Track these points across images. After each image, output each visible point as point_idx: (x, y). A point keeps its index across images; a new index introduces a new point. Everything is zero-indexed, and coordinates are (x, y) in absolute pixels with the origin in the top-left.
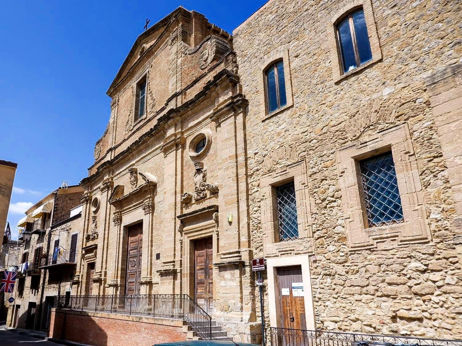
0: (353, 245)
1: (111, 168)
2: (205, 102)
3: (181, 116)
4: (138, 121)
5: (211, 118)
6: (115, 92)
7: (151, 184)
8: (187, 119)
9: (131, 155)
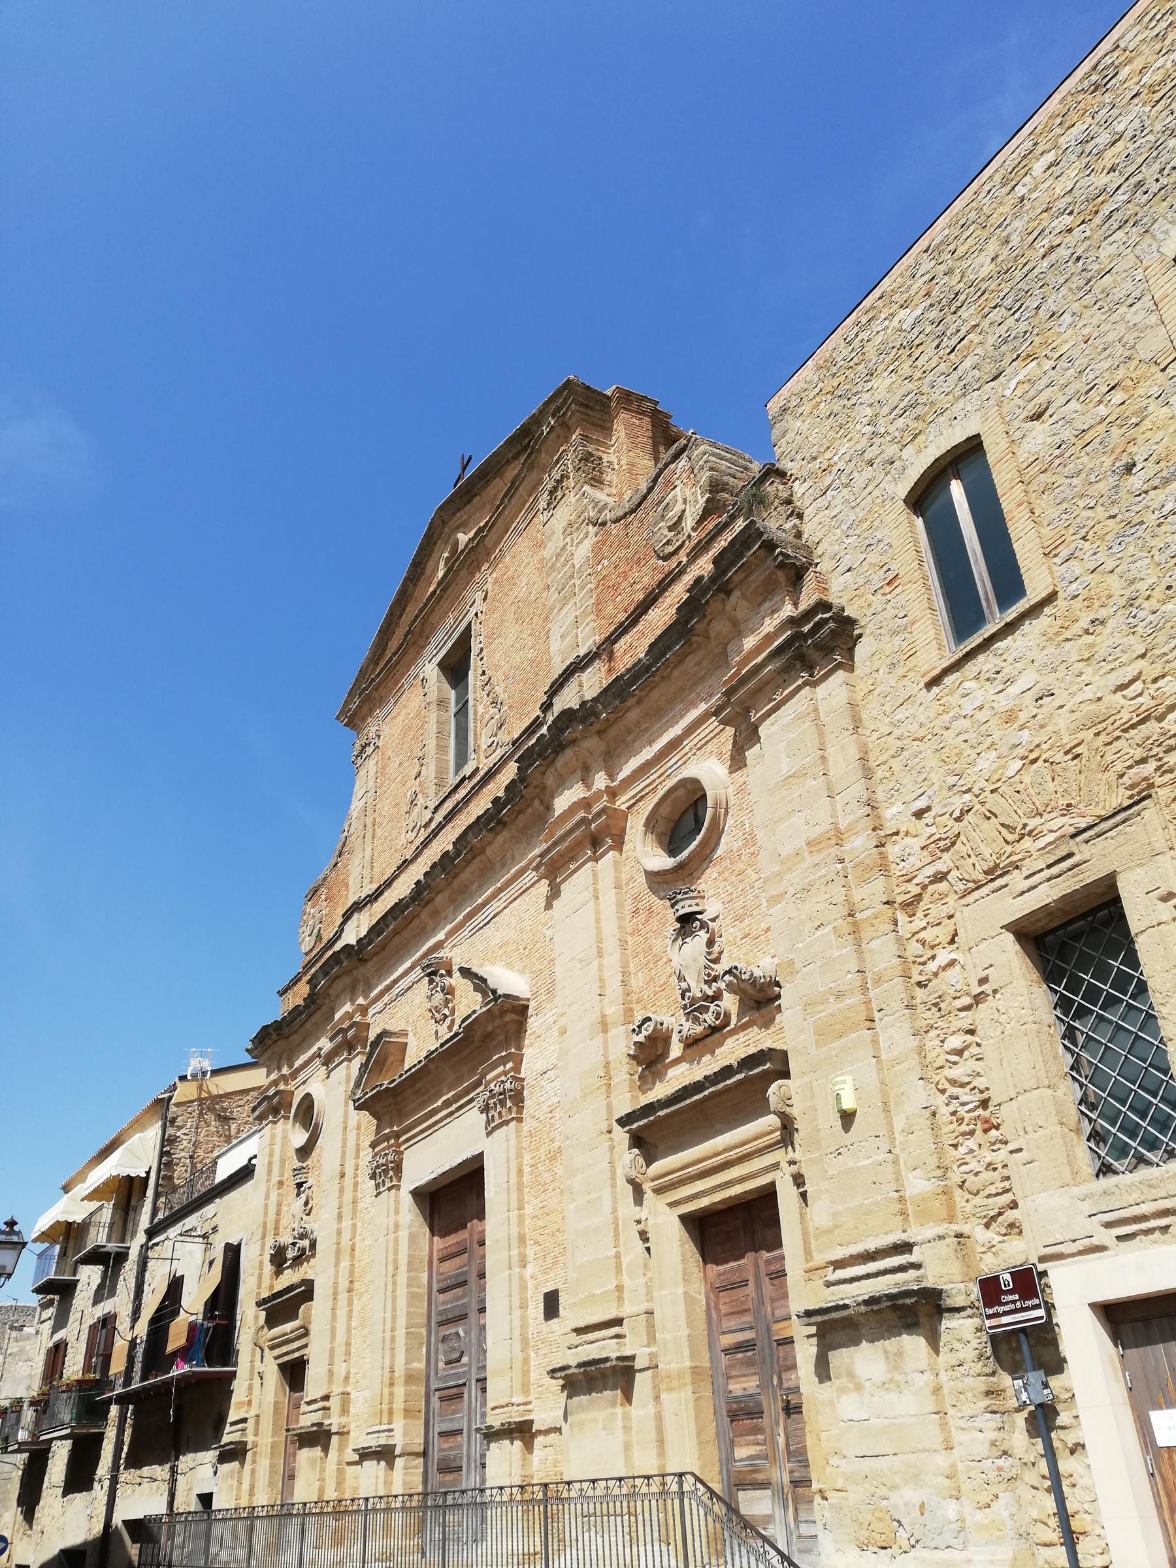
2: (690, 661)
3: (600, 733)
6: (365, 709)
7: (506, 1006)
8: (623, 741)
9: (427, 911)
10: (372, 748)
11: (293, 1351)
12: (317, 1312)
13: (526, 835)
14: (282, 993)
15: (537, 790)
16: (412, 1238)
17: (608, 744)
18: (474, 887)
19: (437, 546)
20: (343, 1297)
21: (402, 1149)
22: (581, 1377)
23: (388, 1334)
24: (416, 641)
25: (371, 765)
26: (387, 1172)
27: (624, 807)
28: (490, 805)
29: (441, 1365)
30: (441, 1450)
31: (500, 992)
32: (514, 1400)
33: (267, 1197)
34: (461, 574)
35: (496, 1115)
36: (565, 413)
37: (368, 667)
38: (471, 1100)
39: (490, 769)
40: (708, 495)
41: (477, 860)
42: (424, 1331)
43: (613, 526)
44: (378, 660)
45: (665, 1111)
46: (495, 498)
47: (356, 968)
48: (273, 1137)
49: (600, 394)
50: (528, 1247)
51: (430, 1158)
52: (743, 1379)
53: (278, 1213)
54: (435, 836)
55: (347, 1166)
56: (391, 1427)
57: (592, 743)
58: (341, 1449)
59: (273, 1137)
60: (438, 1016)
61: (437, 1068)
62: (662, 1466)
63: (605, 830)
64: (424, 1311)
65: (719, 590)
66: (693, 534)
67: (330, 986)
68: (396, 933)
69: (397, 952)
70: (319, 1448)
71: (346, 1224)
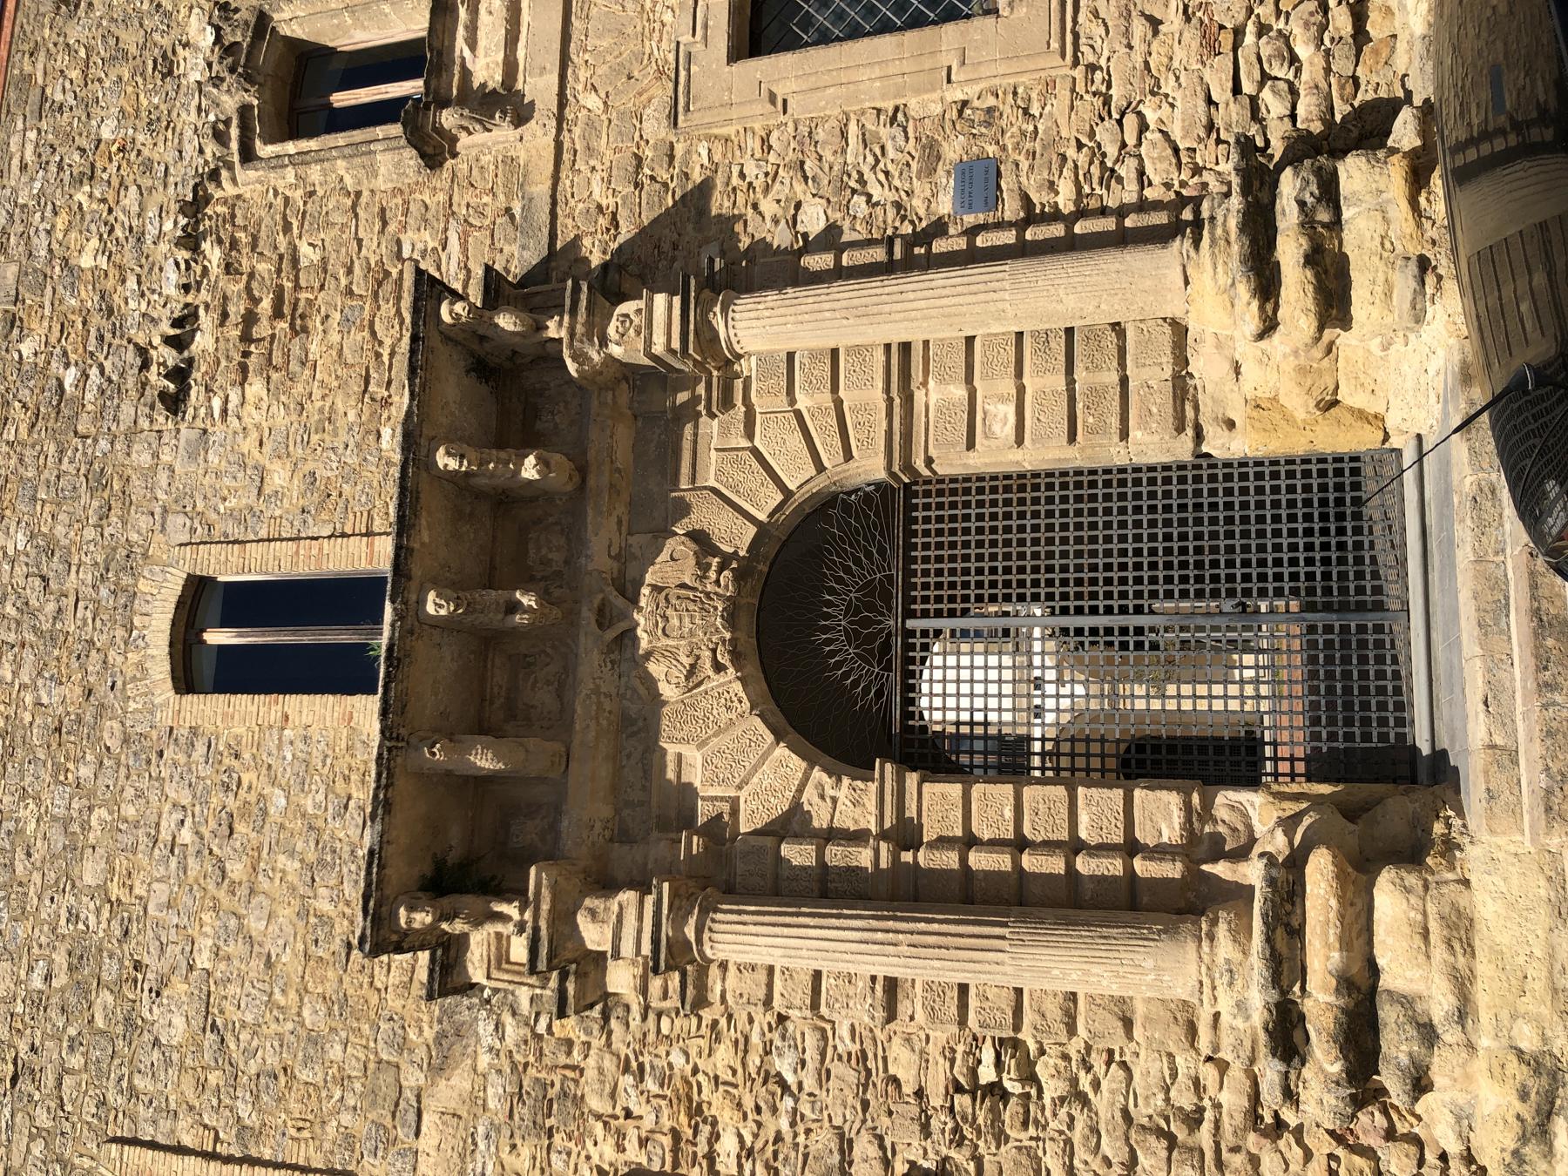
0: (1055, 45)
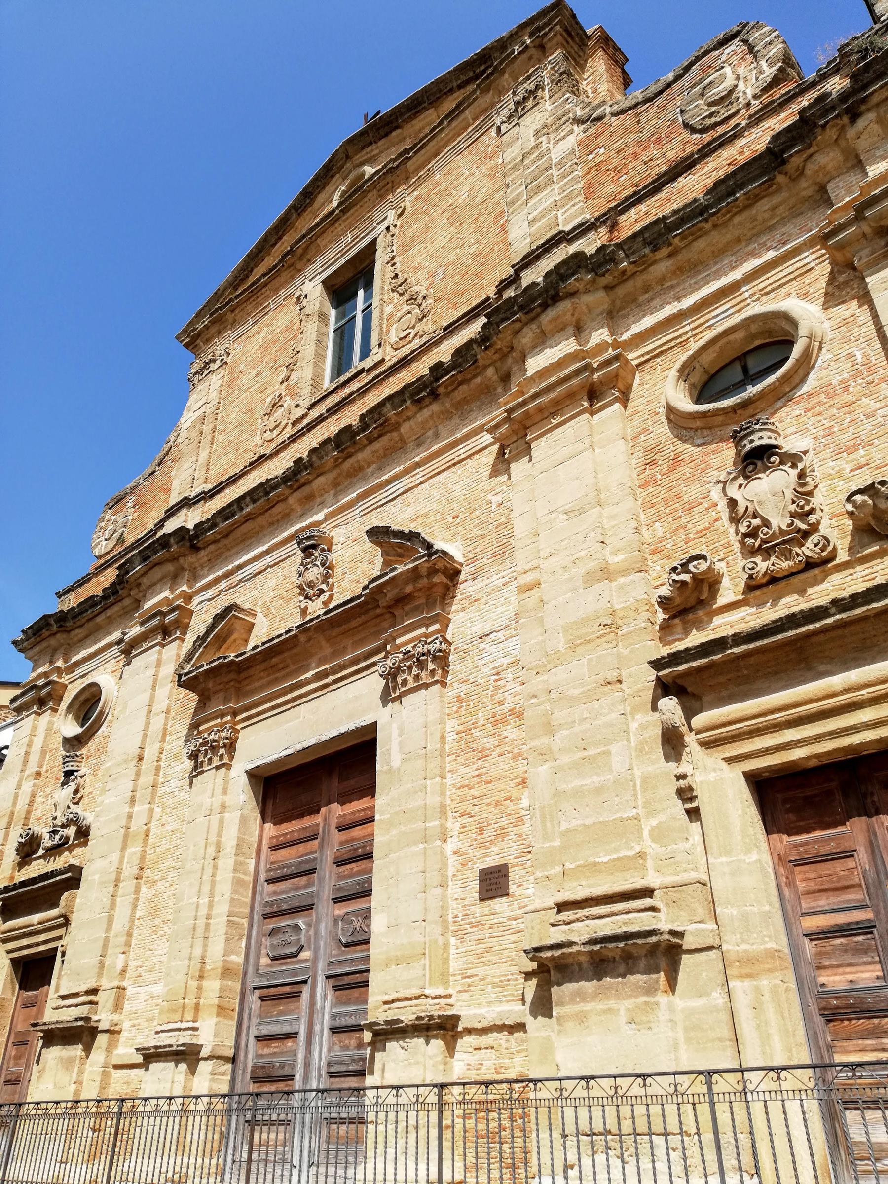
1: (191, 559)
2: (764, 205)
3: (608, 288)
4: (342, 379)
5: (490, 431)
6: (213, 330)
7: (440, 565)
8: (635, 300)
9: (298, 495)
10: (218, 363)
11: (38, 944)
12: (84, 903)
13: (487, 395)
14: (59, 595)
15: (497, 356)
16: (244, 821)
17: (613, 302)
18: (371, 469)
19: (334, 180)
20: (127, 885)
21: (238, 727)
22: (583, 958)
23: (201, 922)
24: (295, 262)
25: (215, 381)
26: (207, 753)
27: (634, 363)
28: (427, 372)
29: (264, 961)
30: (258, 1056)
31: (436, 547)
32: (427, 992)
33: (19, 787)
34: (370, 195)
35: (410, 679)
36: (546, 34)
37: (225, 289)
38: (374, 664)
39: (406, 356)
40: (780, 64)
41: (385, 438)
42: (245, 922)
43: (613, 119)
44: (238, 285)
45: (744, 647)
46: (420, 131)
47: (184, 556)
48: (34, 728)
49: (581, 28)
50: (451, 820)
51: (280, 734)
52: (848, 969)
53: (31, 804)
54: (309, 430)
55: (147, 750)
56: (196, 1025)
57: (597, 299)
58: (109, 1050)
59: (34, 728)
60: (307, 591)
61: (309, 640)
62: (77, 1092)
63: (612, 381)
64: (248, 900)
65: (847, 111)
66: (753, 102)
67: (145, 573)
68: (249, 518)
69: (244, 540)
70: (80, 1046)
71: (140, 808)
